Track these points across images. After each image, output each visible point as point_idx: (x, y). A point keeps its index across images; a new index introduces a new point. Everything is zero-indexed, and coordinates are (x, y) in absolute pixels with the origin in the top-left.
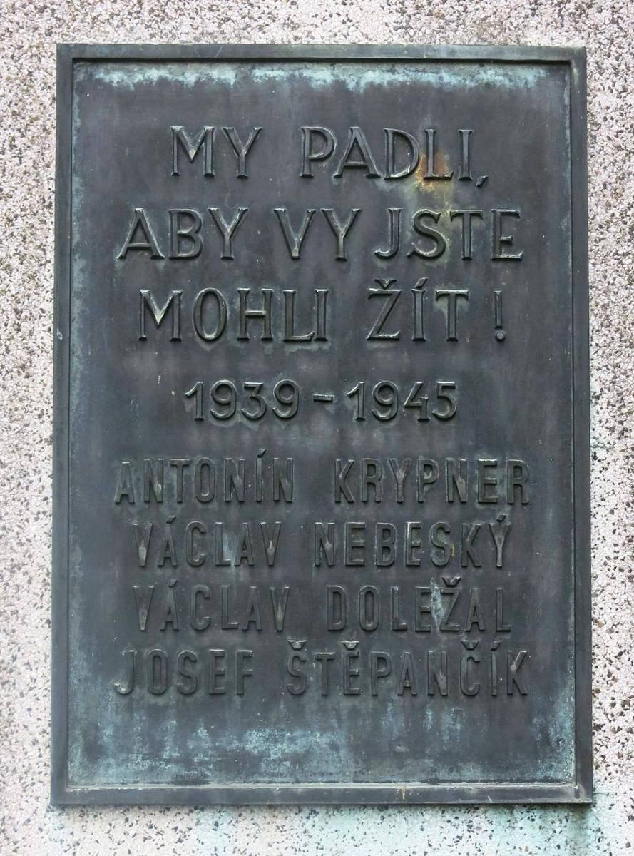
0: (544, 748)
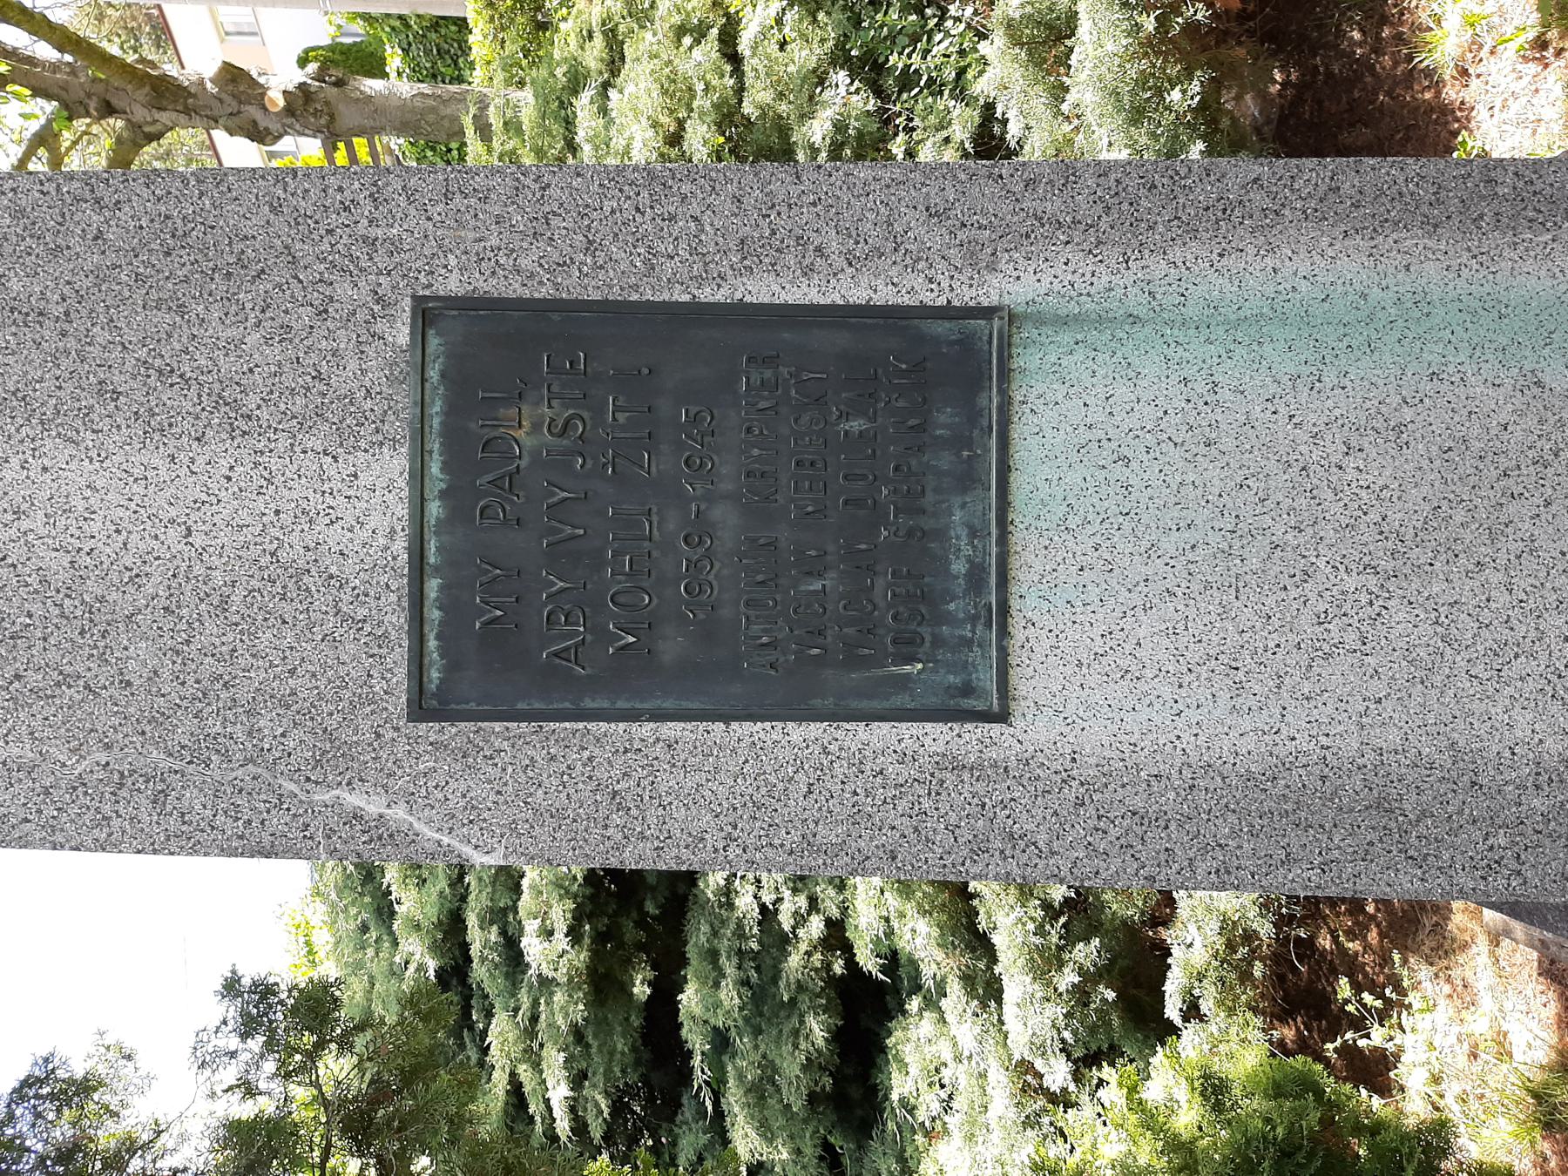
0: (966, 344)
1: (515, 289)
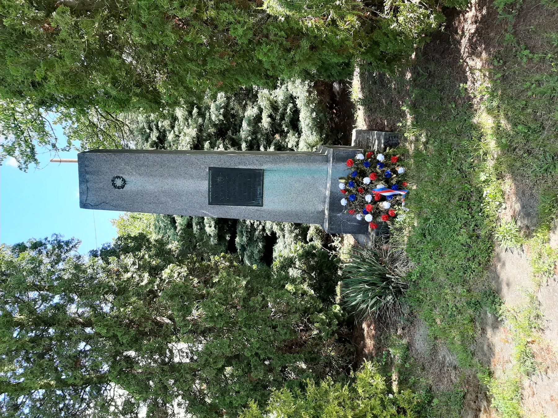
0: (260, 172)
1: (218, 166)
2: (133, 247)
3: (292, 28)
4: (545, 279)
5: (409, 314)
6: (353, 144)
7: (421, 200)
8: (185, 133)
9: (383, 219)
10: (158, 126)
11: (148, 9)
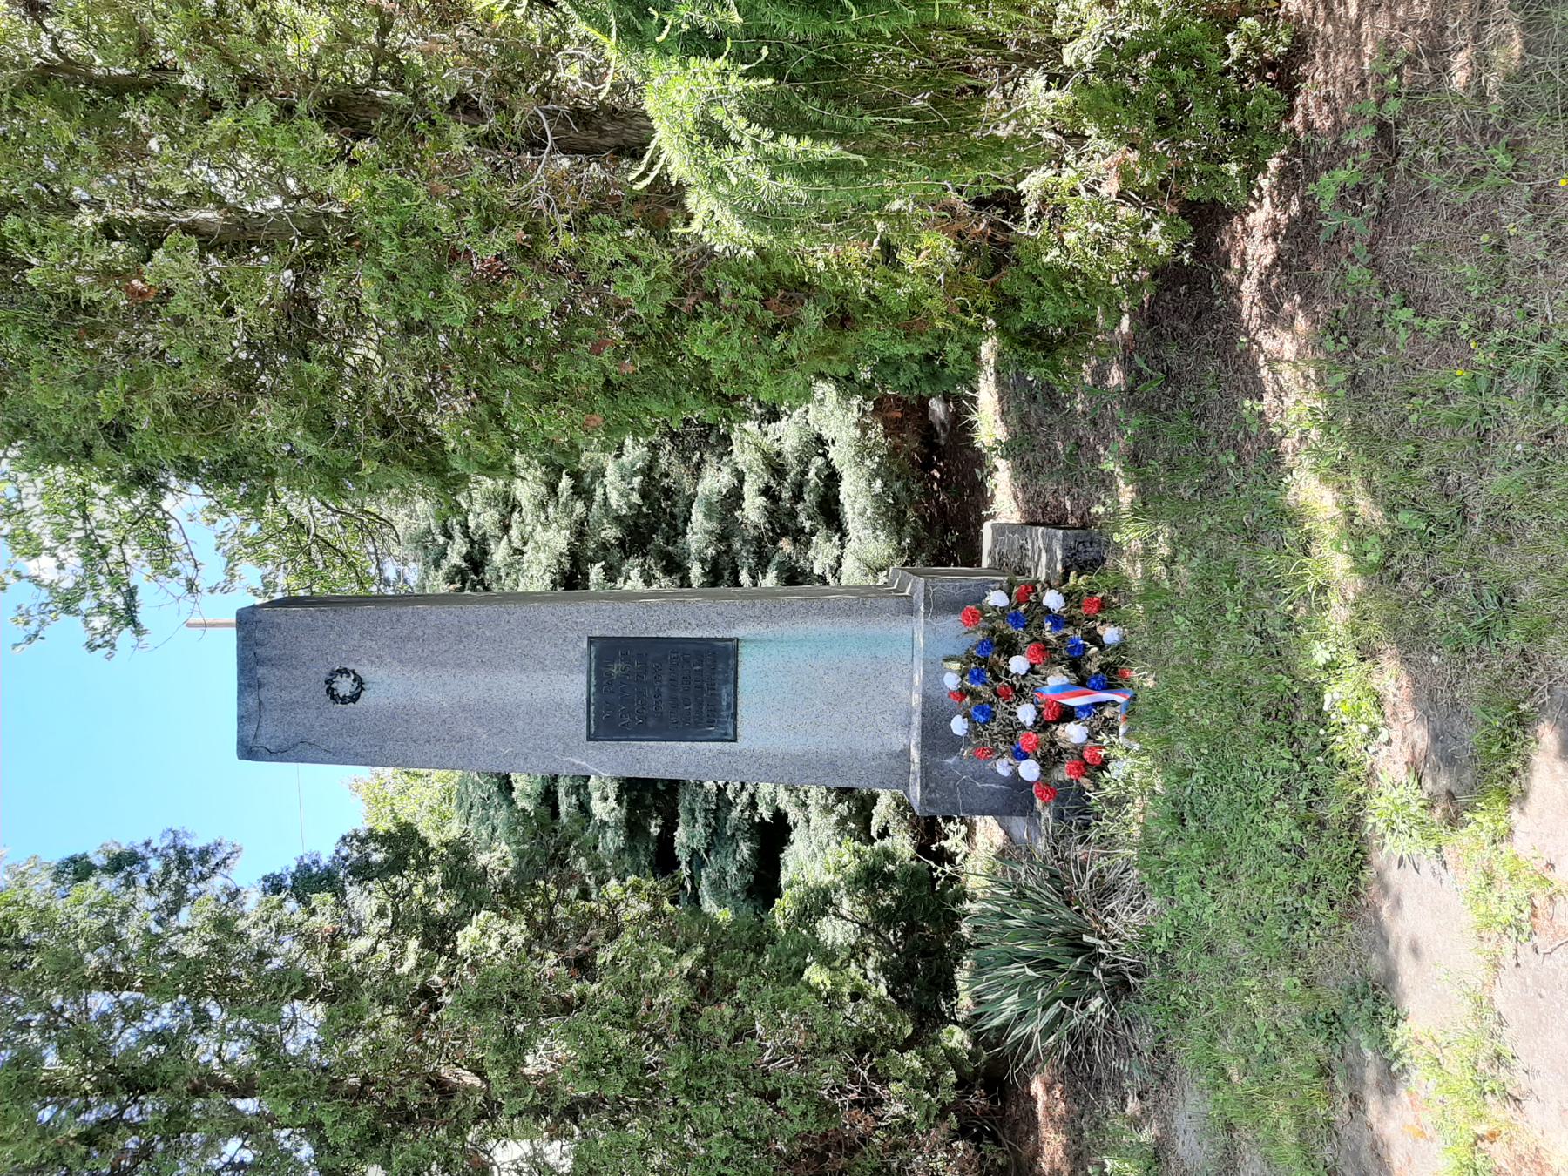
0: (726, 648)
2: (380, 865)
3: (777, 276)
4: (1509, 946)
5: (1154, 1053)
6: (986, 562)
7: (1166, 719)
8: (537, 543)
9: (1070, 773)
10: (468, 527)
11: (402, 233)
